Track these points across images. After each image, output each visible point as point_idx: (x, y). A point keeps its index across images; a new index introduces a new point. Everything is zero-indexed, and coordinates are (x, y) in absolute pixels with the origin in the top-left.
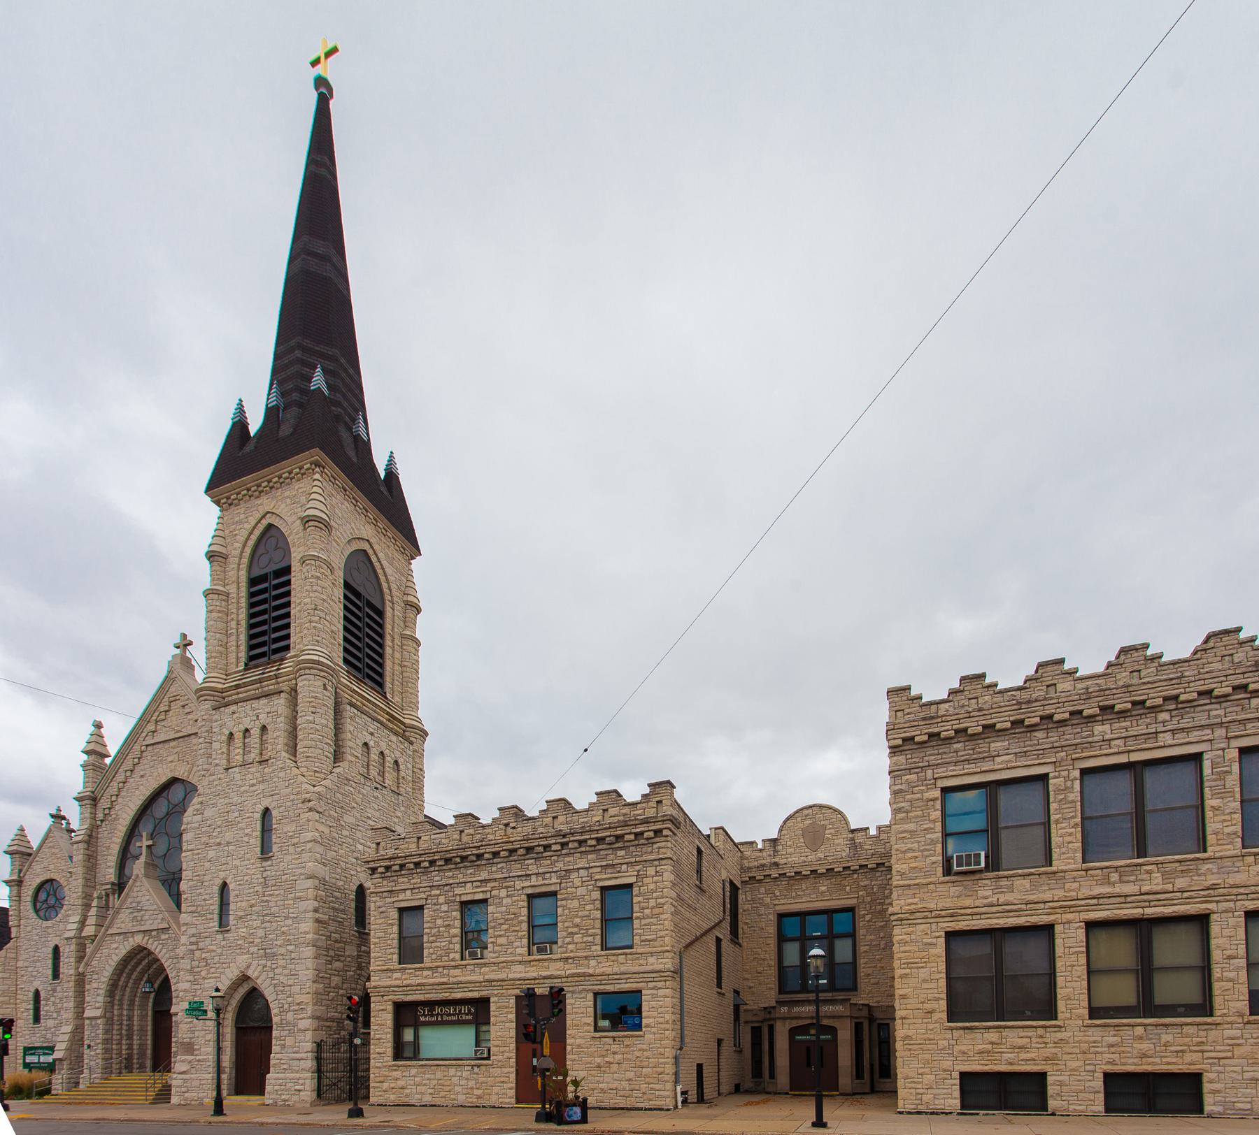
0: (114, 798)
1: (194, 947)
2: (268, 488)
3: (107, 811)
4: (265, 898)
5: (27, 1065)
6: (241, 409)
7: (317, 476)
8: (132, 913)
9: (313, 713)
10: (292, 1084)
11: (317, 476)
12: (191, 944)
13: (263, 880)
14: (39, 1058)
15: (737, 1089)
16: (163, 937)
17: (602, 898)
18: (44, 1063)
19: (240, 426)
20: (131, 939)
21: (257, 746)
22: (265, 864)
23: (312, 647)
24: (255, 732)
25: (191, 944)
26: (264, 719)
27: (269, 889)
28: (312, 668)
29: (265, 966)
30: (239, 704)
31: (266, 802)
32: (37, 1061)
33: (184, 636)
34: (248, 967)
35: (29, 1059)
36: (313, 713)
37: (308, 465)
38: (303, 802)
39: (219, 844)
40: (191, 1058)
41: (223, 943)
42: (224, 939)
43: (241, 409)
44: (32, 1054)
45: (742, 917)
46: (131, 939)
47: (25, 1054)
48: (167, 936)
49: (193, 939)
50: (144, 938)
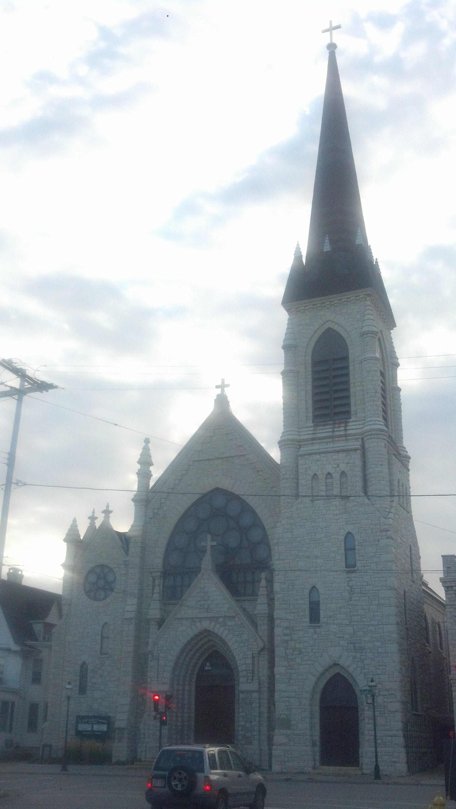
0: (163, 501)
1: (286, 638)
2: (329, 306)
3: (156, 511)
4: (351, 602)
5: (79, 733)
6: (298, 245)
7: (368, 303)
8: (200, 601)
9: (381, 465)
10: (387, 757)
11: (368, 303)
12: (285, 635)
13: (349, 588)
14: (92, 727)
15: (181, 744)
16: (229, 623)
17: (345, 553)
18: (97, 731)
19: (298, 257)
20: (198, 624)
21: (339, 486)
22: (350, 575)
23: (375, 419)
24: (336, 476)
25: (285, 635)
26: (343, 467)
27: (355, 595)
28: (380, 434)
29: (354, 657)
30: (322, 455)
31: (349, 528)
32: (90, 729)
33: (223, 380)
34: (340, 657)
35: (82, 727)
36: (381, 465)
37: (363, 296)
38: (382, 531)
39: (308, 557)
40: (289, 732)
41: (315, 636)
42: (315, 633)
43: (298, 245)
44: (85, 723)
45: (123, 490)
46: (198, 624)
47: (77, 722)
48: (233, 623)
49: (287, 631)
50: (210, 623)
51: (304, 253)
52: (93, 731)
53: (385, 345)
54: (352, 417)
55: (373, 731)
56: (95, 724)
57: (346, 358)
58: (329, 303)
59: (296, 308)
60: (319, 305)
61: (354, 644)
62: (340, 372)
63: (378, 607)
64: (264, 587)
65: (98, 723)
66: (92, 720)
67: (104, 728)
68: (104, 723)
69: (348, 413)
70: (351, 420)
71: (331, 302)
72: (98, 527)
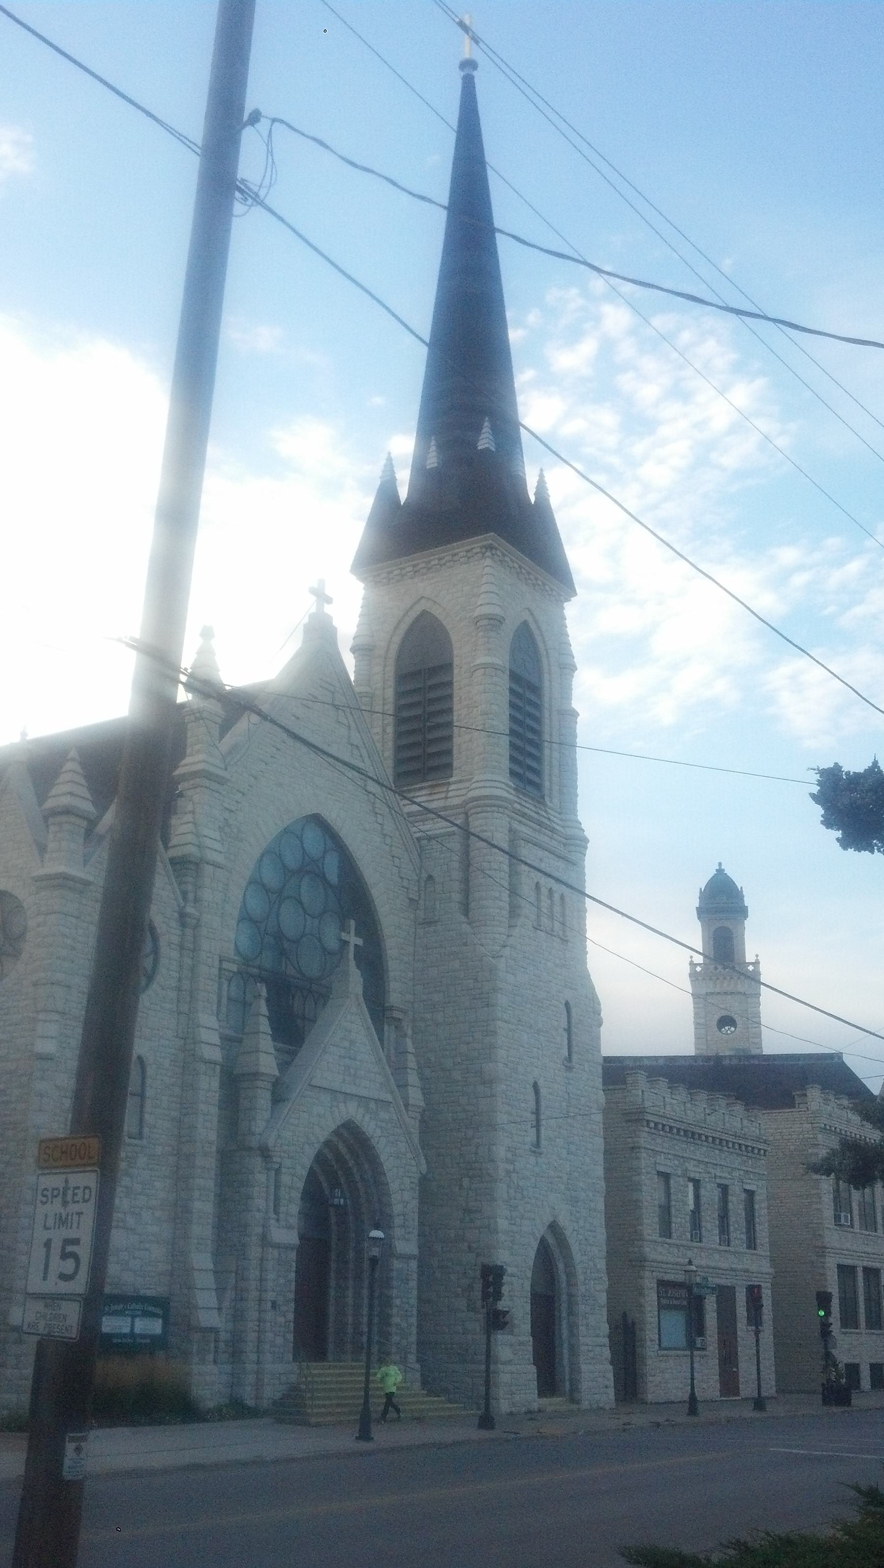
44: (115, 1313)
51: (403, 493)
52: (132, 1335)
53: (56, 1174)
54: (455, 772)
55: (768, 1398)
56: (138, 1315)
57: (447, 667)
58: (436, 562)
59: (388, 573)
60: (423, 565)
61: (574, 1230)
62: (439, 693)
63: (568, 1179)
64: (210, 1270)
65: (146, 1314)
66: (134, 1306)
67: (155, 1327)
68: (154, 1315)
69: (449, 766)
70: (452, 780)
71: (440, 559)
72: (521, 431)
